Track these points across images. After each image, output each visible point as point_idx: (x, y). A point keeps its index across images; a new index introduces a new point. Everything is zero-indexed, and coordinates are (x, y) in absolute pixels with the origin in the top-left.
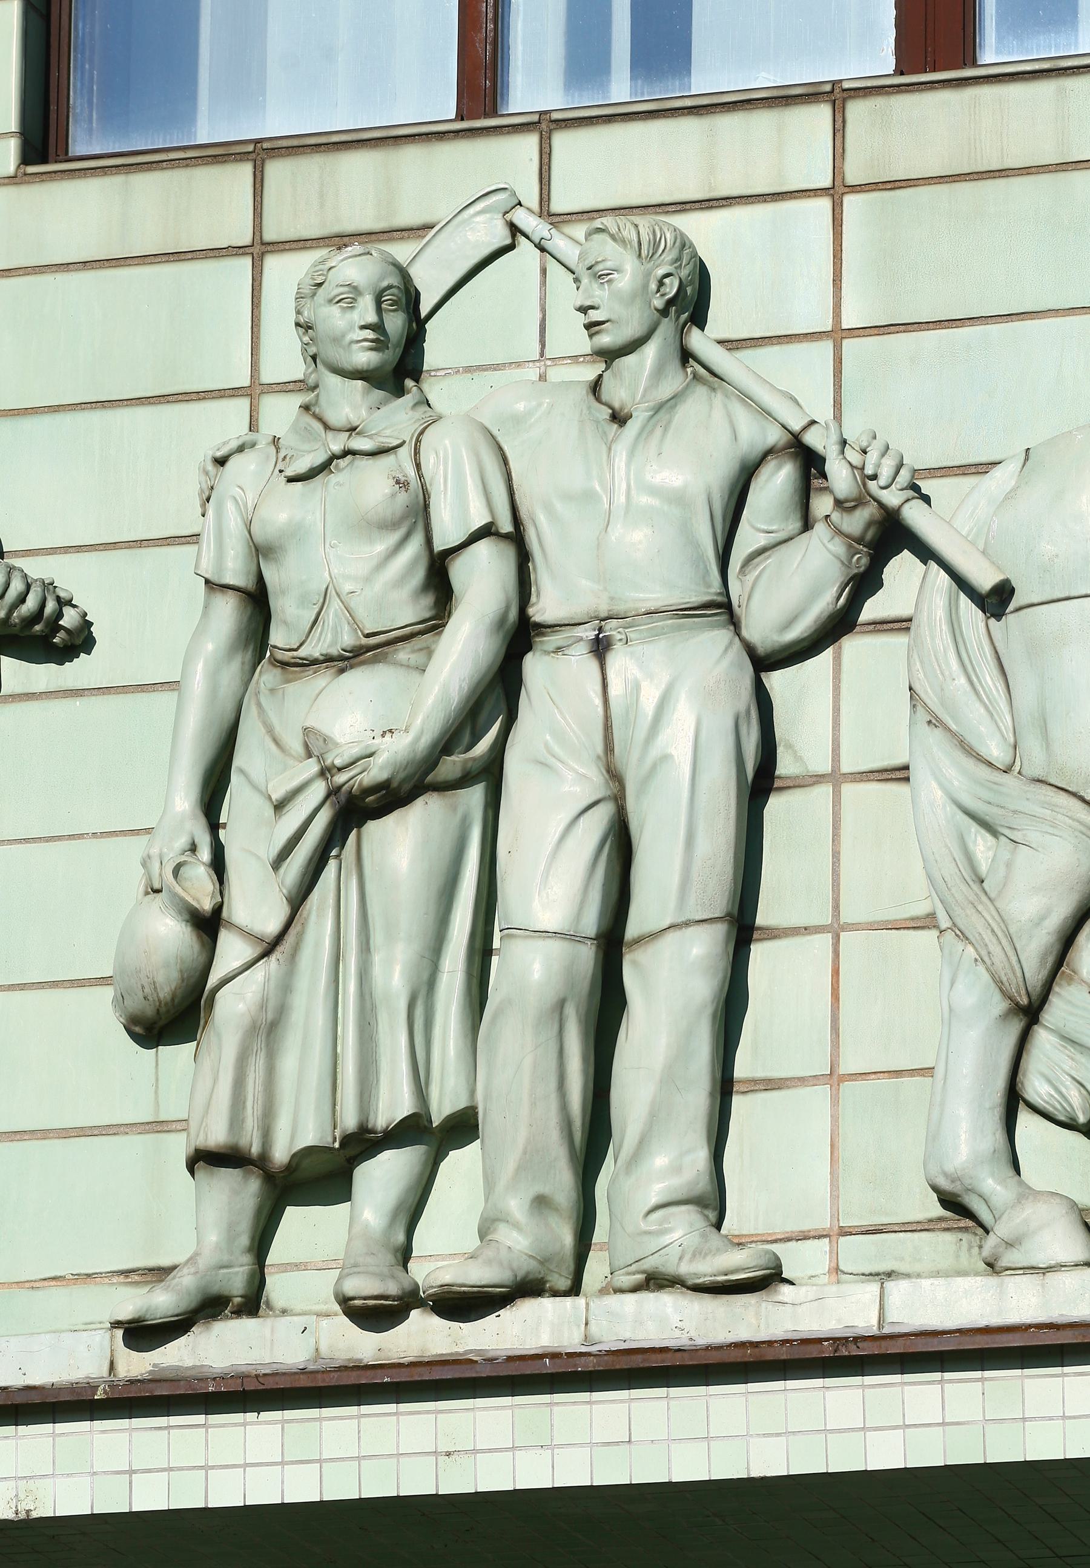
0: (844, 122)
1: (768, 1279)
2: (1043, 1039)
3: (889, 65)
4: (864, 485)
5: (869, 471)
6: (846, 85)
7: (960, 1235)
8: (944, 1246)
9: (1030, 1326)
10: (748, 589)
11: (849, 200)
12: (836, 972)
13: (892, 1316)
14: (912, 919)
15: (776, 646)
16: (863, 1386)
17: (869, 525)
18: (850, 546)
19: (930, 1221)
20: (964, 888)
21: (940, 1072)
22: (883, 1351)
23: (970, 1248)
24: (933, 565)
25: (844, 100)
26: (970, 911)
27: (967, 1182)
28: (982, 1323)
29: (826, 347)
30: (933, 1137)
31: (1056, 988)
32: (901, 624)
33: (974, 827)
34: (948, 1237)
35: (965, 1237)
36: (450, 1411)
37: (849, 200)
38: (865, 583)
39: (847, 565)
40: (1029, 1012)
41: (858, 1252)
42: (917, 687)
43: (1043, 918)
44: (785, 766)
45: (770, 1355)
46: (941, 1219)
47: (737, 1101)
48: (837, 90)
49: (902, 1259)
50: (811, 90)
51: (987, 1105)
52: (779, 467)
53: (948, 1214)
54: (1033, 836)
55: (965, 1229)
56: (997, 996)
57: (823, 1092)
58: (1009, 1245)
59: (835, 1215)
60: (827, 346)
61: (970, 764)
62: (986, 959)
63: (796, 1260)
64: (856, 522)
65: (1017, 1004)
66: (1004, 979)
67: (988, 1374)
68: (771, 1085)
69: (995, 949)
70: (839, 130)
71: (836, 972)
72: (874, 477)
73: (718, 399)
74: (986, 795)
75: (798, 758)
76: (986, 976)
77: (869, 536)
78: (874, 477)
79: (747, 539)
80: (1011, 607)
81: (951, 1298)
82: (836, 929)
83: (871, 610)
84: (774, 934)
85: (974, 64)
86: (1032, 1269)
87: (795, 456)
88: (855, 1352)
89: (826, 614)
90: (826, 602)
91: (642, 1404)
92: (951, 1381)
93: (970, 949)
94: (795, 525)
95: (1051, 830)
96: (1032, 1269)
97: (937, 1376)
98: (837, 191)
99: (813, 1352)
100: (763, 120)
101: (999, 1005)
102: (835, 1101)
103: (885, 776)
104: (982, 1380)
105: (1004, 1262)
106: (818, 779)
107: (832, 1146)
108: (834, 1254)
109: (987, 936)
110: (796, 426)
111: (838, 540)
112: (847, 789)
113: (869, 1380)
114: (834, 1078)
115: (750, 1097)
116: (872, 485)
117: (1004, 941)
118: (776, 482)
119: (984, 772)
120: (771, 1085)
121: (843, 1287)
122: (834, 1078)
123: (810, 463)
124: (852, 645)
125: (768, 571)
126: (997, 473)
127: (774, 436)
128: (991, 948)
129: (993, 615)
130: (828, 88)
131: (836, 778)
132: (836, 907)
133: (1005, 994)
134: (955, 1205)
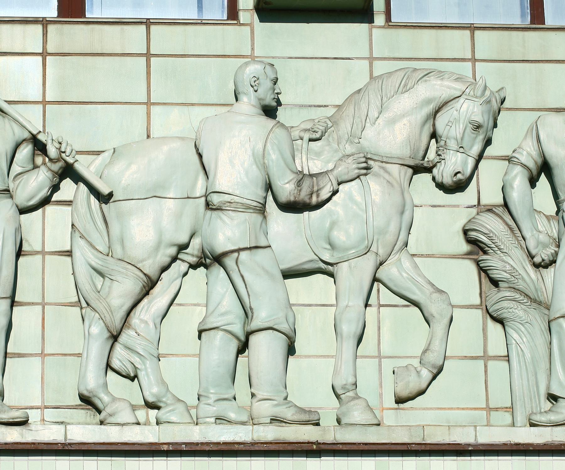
0: (47, 31)
1: (23, 423)
2: (118, 348)
3: (55, 14)
4: (60, 155)
5: (63, 150)
6: (48, 19)
7: (87, 411)
8: (84, 414)
9: (119, 443)
10: (16, 186)
11: (48, 58)
12: (43, 319)
13: (69, 437)
14: (70, 303)
15: (25, 206)
16: (69, 460)
17: (61, 168)
18: (54, 175)
19: (76, 405)
20: (93, 293)
21: (85, 355)
22: (80, 449)
23: (90, 416)
24: (81, 185)
25: (47, 24)
26: (97, 302)
27: (94, 393)
28: (102, 441)
29: (41, 106)
30: (82, 377)
31: (124, 330)
32: (69, 203)
33: (95, 274)
34: (83, 411)
35: (89, 412)
36: (408, 460)
37: (48, 58)
38: (55, 188)
39: (52, 181)
40: (115, 338)
41: (49, 414)
42: (76, 224)
43: (122, 306)
44: (25, 248)
45: (40, 447)
46: (80, 405)
47: (7, 359)
48: (44, 21)
49: (67, 418)
50: (35, 19)
51: (101, 368)
52: (27, 146)
53: (83, 404)
54: (119, 278)
55: (89, 409)
56: (106, 331)
57: (39, 359)
58: (111, 415)
59: (43, 401)
60: (41, 106)
61: (95, 252)
62: (104, 318)
63: (34, 416)
64: (56, 167)
65: (113, 335)
66: (109, 326)
67: (113, 458)
68: (20, 355)
69: (106, 315)
70: (45, 34)
71: (43, 319)
72: (64, 152)
73: (6, 120)
74: (100, 263)
75: (30, 245)
76: (103, 324)
77: (60, 172)
78: (64, 152)
79: (16, 169)
80: (112, 200)
81: (84, 431)
82: (43, 305)
83: (55, 197)
84: (21, 304)
85: (85, 17)
86: (118, 424)
87: (32, 142)
88: (257, 449)
89: (43, 197)
90: (44, 193)
91: (46, 461)
92: (239, 460)
93: (97, 314)
94: (31, 166)
95: (126, 277)
96: (118, 424)
97: (96, 458)
98: (44, 54)
99: (55, 447)
100: (18, 28)
101: (107, 334)
102: (43, 363)
103: (61, 254)
104: (111, 460)
105: (108, 421)
106: (37, 253)
107: (42, 378)
108: (43, 414)
109: (104, 311)
110: (35, 132)
111: (49, 172)
112: (47, 257)
113: (71, 458)
114: (43, 355)
115: (13, 359)
116: (63, 155)
117: (110, 313)
118: (26, 151)
119: (100, 255)
120: (20, 355)
121: (46, 426)
122: (43, 355)
123: (40, 147)
124: (49, 209)
125: (23, 182)
126: (103, 155)
127: (26, 135)
128: (106, 315)
129: (104, 203)
130: (41, 19)
131: (43, 253)
132: (43, 297)
133: (109, 331)
134: (87, 401)
